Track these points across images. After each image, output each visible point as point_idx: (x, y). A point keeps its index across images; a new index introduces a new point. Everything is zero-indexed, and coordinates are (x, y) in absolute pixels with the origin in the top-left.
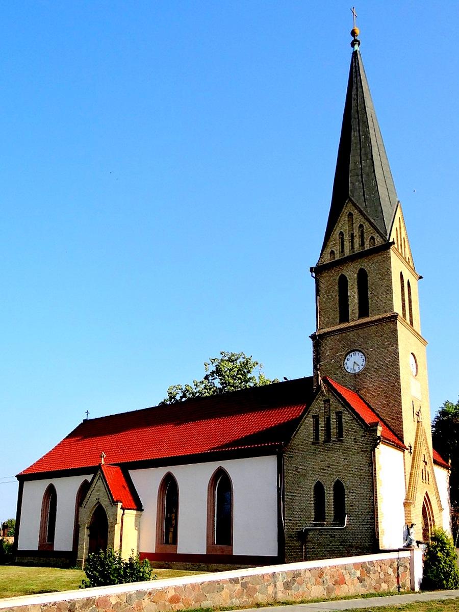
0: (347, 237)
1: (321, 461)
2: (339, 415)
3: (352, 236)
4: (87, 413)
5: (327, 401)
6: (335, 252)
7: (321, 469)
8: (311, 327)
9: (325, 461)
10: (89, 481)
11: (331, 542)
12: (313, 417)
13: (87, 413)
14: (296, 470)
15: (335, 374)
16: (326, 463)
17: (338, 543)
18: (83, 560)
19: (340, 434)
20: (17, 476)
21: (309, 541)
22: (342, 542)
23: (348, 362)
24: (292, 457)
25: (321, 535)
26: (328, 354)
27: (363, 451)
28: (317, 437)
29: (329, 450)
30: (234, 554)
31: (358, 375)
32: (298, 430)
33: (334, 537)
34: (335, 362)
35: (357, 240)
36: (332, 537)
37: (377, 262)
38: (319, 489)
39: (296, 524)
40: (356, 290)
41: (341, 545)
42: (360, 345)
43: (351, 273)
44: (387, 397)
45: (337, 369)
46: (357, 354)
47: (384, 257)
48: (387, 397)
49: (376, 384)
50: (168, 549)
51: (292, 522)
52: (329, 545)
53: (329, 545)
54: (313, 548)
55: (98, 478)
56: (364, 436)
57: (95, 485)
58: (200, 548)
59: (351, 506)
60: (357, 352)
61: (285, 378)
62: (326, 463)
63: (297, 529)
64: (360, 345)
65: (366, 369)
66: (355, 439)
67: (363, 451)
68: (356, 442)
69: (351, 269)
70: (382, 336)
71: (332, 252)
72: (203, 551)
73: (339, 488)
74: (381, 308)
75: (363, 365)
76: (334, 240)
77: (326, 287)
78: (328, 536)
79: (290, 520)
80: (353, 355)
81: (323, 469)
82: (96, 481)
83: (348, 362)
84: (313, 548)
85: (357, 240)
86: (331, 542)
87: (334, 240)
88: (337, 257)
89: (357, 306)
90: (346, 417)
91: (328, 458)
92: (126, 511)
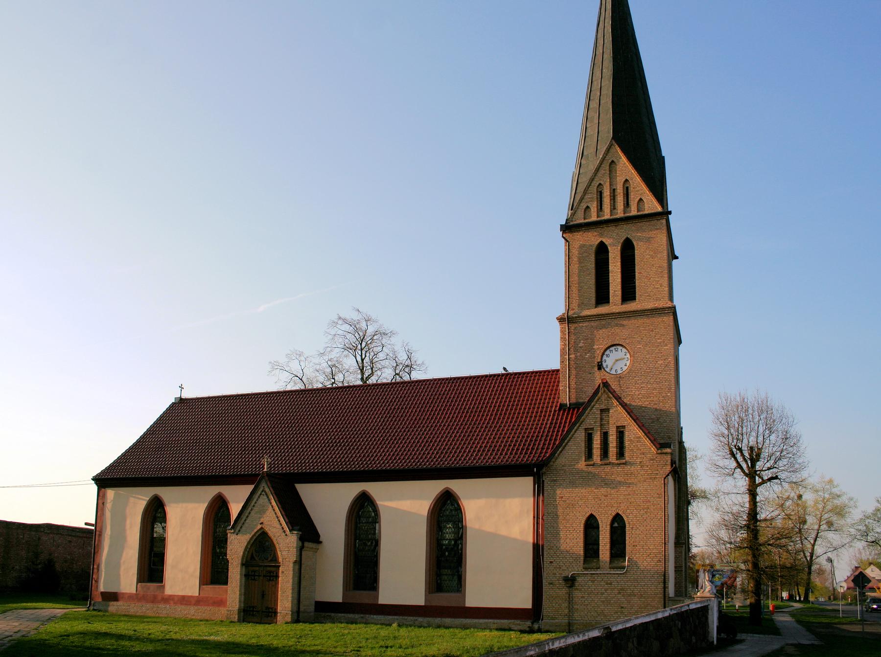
0: (607, 193)
2: (621, 434)
3: (613, 192)
4: (181, 387)
8: (561, 309)
13: (181, 387)
15: (590, 374)
17: (616, 591)
18: (858, 593)
19: (621, 454)
21: (577, 589)
23: (607, 359)
24: (555, 481)
25: (593, 581)
26: (581, 345)
27: (651, 478)
32: (565, 446)
33: (611, 584)
35: (620, 199)
36: (607, 584)
38: (591, 524)
40: (619, 264)
41: (619, 593)
46: (619, 350)
50: (444, 599)
51: (554, 564)
52: (602, 594)
53: (602, 594)
54: (583, 597)
55: (259, 493)
57: (256, 503)
58: (416, 595)
60: (620, 348)
61: (505, 369)
65: (630, 371)
66: (640, 462)
67: (651, 478)
69: (614, 235)
70: (652, 331)
72: (421, 601)
73: (618, 526)
74: (652, 294)
75: (628, 365)
78: (603, 583)
79: (551, 562)
80: (614, 351)
82: (257, 497)
83: (607, 359)
84: (583, 597)
85: (620, 199)
86: (606, 590)
88: (594, 218)
89: (619, 287)
92: (306, 544)
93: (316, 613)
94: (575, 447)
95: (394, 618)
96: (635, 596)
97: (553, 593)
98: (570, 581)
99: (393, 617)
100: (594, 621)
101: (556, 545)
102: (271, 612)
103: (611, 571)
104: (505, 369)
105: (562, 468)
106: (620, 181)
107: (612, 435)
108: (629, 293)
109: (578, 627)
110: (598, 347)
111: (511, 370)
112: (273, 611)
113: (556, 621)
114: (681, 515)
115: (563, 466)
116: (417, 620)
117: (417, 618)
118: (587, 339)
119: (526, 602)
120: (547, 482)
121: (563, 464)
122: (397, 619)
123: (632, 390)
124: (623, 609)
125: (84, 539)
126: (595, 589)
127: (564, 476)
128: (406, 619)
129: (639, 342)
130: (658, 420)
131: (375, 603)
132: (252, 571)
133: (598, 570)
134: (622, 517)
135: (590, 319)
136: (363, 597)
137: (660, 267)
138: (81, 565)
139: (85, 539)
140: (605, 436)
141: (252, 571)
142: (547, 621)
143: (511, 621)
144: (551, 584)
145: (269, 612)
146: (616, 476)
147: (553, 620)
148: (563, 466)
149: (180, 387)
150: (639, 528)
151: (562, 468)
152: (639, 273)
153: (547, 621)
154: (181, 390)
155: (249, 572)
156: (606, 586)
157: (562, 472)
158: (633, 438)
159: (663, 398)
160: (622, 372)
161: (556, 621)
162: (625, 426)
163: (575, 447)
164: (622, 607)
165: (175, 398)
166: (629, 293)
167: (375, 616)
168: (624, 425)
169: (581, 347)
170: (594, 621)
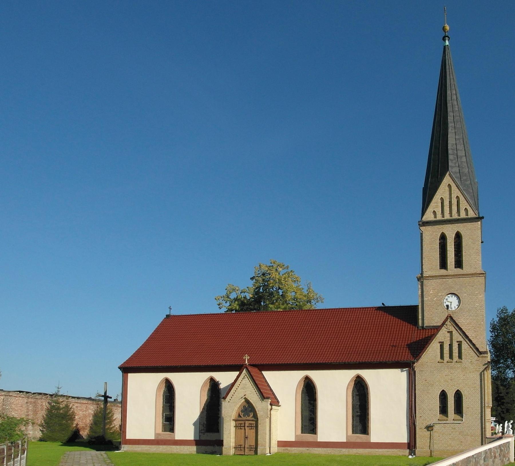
1: (445, 376)
4: (170, 308)
5: (451, 333)
6: (437, 213)
7: (445, 381)
9: (448, 376)
10: (406, 371)
11: (452, 432)
12: (440, 342)
13: (170, 308)
14: (425, 380)
15: (437, 309)
16: (449, 377)
17: (458, 433)
19: (460, 357)
20: (119, 368)
22: (461, 432)
28: (442, 357)
29: (451, 368)
30: (371, 442)
31: (455, 312)
34: (437, 300)
37: (470, 229)
38: (443, 396)
39: (426, 420)
42: (456, 290)
43: (450, 231)
44: (475, 331)
45: (438, 306)
47: (475, 227)
48: (475, 331)
49: (468, 321)
50: (167, 435)
51: (422, 418)
54: (439, 436)
56: (478, 360)
59: (467, 408)
61: (383, 304)
62: (449, 377)
63: (427, 423)
64: (456, 290)
66: (471, 362)
67: (476, 371)
68: (472, 364)
70: (473, 286)
71: (434, 212)
73: (458, 396)
75: (445, 300)
76: (436, 203)
77: (430, 239)
78: (450, 428)
79: (421, 417)
80: (450, 297)
81: (447, 381)
84: (439, 436)
86: (452, 432)
87: (436, 203)
90: (465, 346)
91: (451, 373)
93: (279, 448)
94: (433, 352)
95: (328, 450)
96: (468, 435)
97: (421, 434)
98: (429, 428)
99: (327, 449)
100: (446, 450)
101: (423, 407)
102: (253, 448)
103: (455, 422)
104: (383, 304)
105: (426, 364)
106: (454, 196)
107: (455, 346)
108: (459, 264)
109: (437, 453)
110: (441, 294)
111: (387, 304)
112: (237, 449)
113: (424, 449)
114: (489, 391)
115: (426, 363)
116: (342, 450)
117: (342, 449)
118: (435, 289)
119: (404, 439)
120: (417, 372)
121: (426, 362)
122: (329, 450)
123: (461, 320)
124: (462, 443)
125: (86, 405)
126: (446, 432)
127: (427, 368)
128: (335, 450)
129: (465, 293)
130: (476, 337)
131: (315, 441)
132: (239, 424)
133: (448, 421)
134: (461, 392)
135: (437, 278)
136: (309, 437)
137: (477, 249)
138: (85, 422)
139: (87, 405)
140: (451, 346)
141: (239, 424)
142: (419, 450)
143: (398, 450)
144: (421, 429)
145: (251, 448)
146: (457, 369)
147: (422, 449)
148: (426, 363)
149: (169, 308)
150: (470, 398)
151: (426, 364)
152: (465, 252)
153: (419, 450)
154: (170, 310)
155: (237, 424)
156: (452, 430)
157: (426, 366)
158: (466, 348)
159: (479, 325)
160: (455, 309)
161: (424, 449)
162: (461, 341)
163: (433, 352)
164: (461, 442)
165: (166, 315)
166: (459, 264)
167: (316, 449)
168: (461, 340)
169: (431, 294)
170: (446, 450)
